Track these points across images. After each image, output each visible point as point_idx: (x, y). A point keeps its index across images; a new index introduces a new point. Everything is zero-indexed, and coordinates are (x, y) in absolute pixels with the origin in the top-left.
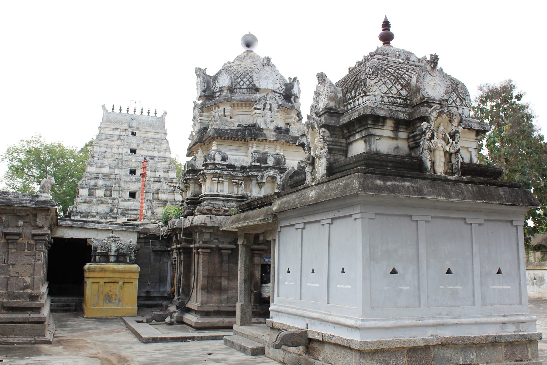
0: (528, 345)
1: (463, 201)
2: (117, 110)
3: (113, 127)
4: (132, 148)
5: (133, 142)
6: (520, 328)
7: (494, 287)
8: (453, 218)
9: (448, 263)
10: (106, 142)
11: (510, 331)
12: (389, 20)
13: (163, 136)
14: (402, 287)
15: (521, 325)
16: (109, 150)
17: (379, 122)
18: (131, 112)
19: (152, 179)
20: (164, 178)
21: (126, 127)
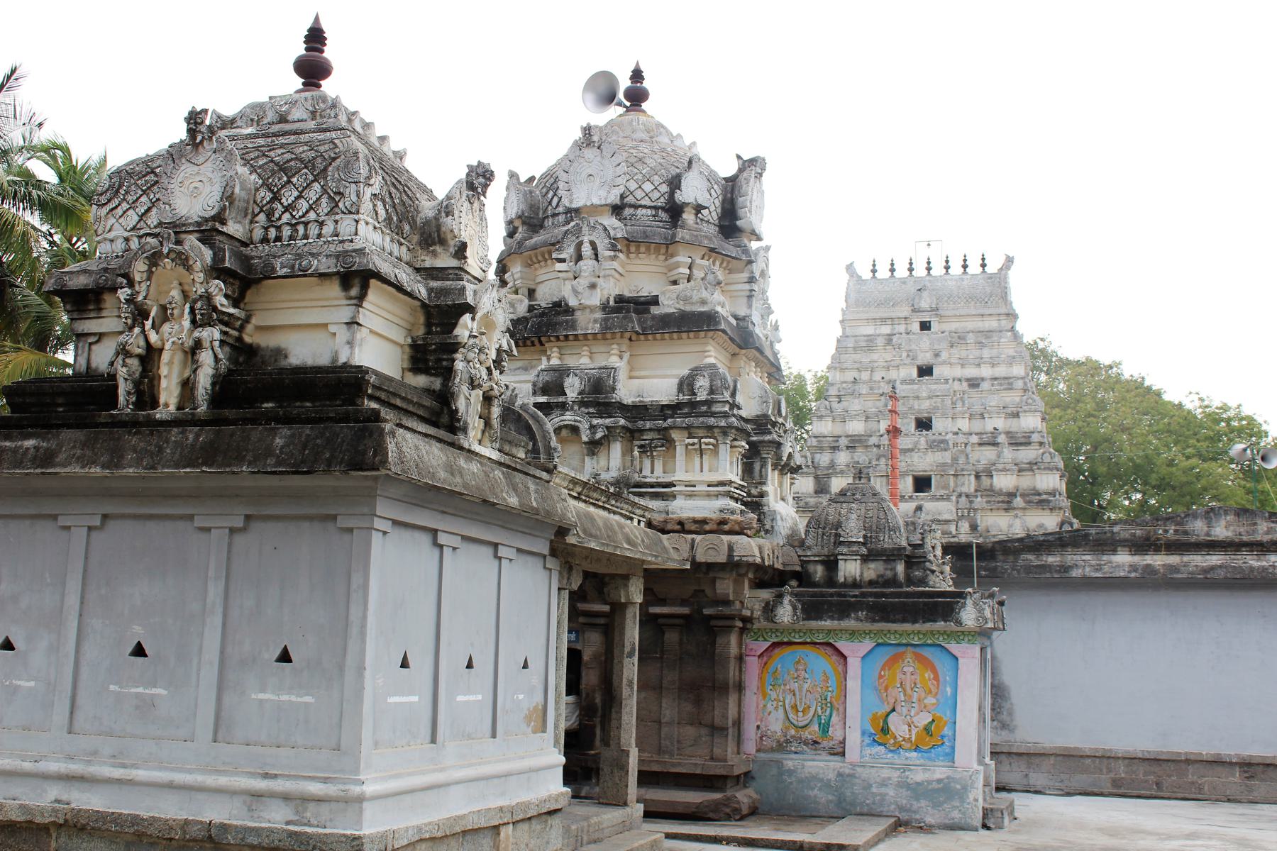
1: (150, 473)
2: (883, 273)
4: (920, 362)
5: (923, 347)
6: (308, 815)
7: (262, 696)
9: (137, 629)
10: (857, 357)
12: (325, 26)
13: (1003, 323)
14: (19, 683)
15: (311, 806)
16: (865, 376)
17: (87, 302)
18: (920, 271)
19: (975, 439)
20: (1007, 433)
21: (904, 311)
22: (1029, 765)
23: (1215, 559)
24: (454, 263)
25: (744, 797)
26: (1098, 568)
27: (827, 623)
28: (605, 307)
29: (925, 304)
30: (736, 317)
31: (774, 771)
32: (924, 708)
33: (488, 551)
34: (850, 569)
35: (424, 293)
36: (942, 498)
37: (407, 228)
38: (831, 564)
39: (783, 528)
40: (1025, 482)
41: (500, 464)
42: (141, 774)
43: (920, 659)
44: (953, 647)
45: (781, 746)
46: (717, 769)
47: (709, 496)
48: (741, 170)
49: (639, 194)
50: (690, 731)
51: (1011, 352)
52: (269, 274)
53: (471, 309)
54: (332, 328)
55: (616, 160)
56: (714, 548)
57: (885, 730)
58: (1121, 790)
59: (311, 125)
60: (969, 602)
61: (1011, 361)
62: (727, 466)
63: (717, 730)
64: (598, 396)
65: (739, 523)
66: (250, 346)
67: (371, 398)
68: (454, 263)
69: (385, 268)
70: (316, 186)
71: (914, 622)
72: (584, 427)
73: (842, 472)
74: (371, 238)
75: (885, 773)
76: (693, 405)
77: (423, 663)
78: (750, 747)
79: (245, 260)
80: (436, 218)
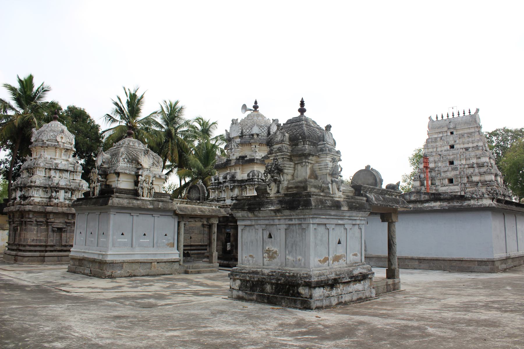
5: (451, 140)
10: (432, 144)
11: (100, 258)
12: (304, 100)
16: (435, 150)
18: (451, 116)
19: (467, 166)
21: (445, 129)
28: (237, 159)
29: (451, 127)
36: (456, 185)
40: (483, 178)
42: (90, 251)
61: (478, 141)
64: (233, 179)
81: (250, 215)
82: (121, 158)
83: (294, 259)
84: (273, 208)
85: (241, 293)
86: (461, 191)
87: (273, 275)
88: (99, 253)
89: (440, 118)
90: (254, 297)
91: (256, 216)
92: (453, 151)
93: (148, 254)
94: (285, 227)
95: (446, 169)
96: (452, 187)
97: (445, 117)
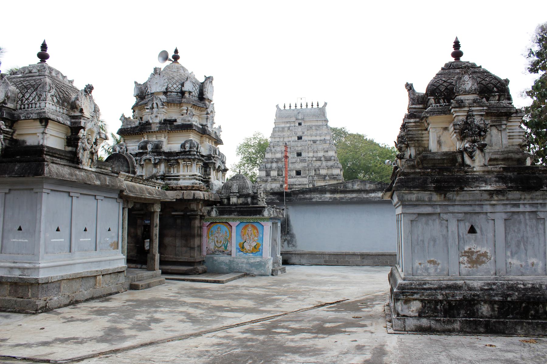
0: (30, 287)
3: (284, 121)
7: (14, 240)
8: (18, 190)
11: (17, 274)
12: (47, 43)
15: (26, 270)
16: (282, 139)
18: (299, 107)
19: (314, 159)
22: (301, 257)
23: (354, 195)
24: (80, 114)
25: (200, 268)
26: (321, 198)
27: (226, 216)
28: (160, 123)
30: (202, 125)
31: (211, 260)
32: (254, 241)
33: (93, 197)
34: (234, 200)
35: (69, 123)
36: (304, 177)
37: (66, 104)
38: (229, 199)
39: (215, 188)
40: (330, 172)
41: (96, 172)
43: (253, 226)
44: (262, 223)
45: (214, 253)
46: (192, 260)
47: (189, 179)
48: (205, 80)
49: (172, 88)
50: (184, 249)
51: (326, 132)
52: (19, 119)
53: (84, 128)
54: (38, 134)
55: (164, 78)
56: (189, 195)
57: (243, 247)
58: (327, 263)
59: (37, 74)
60: (266, 209)
62: (196, 170)
63: (192, 248)
64: (157, 150)
65: (198, 187)
66: (16, 140)
67: (46, 155)
68: (80, 114)
69: (52, 116)
70: (35, 93)
71: (251, 215)
72: (152, 159)
73: (274, 170)
74: (50, 107)
75: (243, 260)
76: (185, 152)
77: (65, 230)
78: (205, 253)
79: (12, 115)
80: (75, 101)
81: (436, 197)
82: (49, 94)
83: (523, 264)
84: (489, 188)
85: (425, 322)
86: (310, 183)
87: (491, 289)
88: (12, 265)
89: (287, 108)
90: (457, 326)
91: (449, 200)
92: (300, 143)
93: (92, 262)
94: (504, 216)
95: (294, 160)
96: (301, 179)
97: (293, 107)
